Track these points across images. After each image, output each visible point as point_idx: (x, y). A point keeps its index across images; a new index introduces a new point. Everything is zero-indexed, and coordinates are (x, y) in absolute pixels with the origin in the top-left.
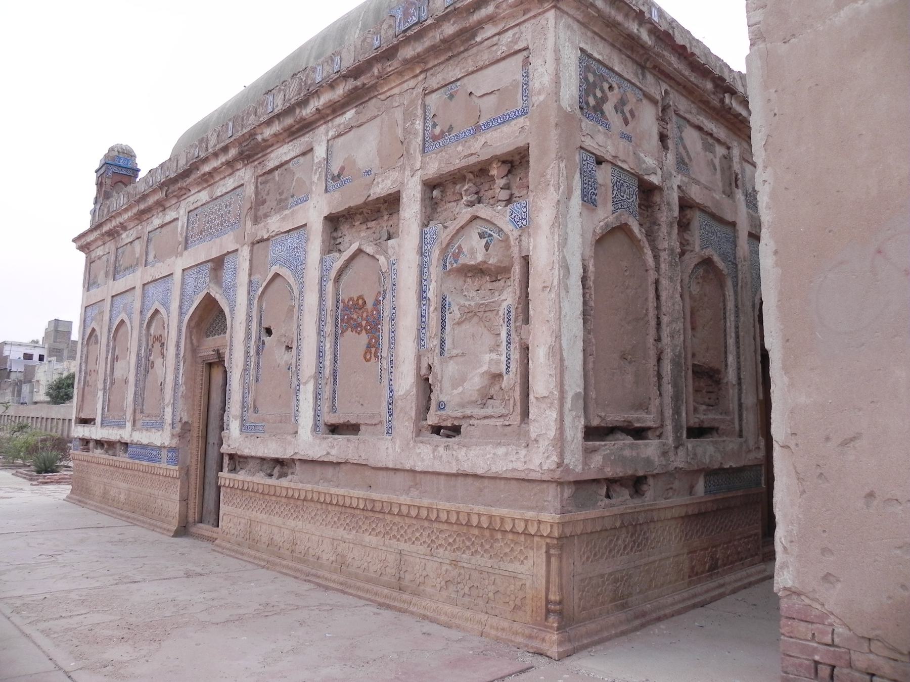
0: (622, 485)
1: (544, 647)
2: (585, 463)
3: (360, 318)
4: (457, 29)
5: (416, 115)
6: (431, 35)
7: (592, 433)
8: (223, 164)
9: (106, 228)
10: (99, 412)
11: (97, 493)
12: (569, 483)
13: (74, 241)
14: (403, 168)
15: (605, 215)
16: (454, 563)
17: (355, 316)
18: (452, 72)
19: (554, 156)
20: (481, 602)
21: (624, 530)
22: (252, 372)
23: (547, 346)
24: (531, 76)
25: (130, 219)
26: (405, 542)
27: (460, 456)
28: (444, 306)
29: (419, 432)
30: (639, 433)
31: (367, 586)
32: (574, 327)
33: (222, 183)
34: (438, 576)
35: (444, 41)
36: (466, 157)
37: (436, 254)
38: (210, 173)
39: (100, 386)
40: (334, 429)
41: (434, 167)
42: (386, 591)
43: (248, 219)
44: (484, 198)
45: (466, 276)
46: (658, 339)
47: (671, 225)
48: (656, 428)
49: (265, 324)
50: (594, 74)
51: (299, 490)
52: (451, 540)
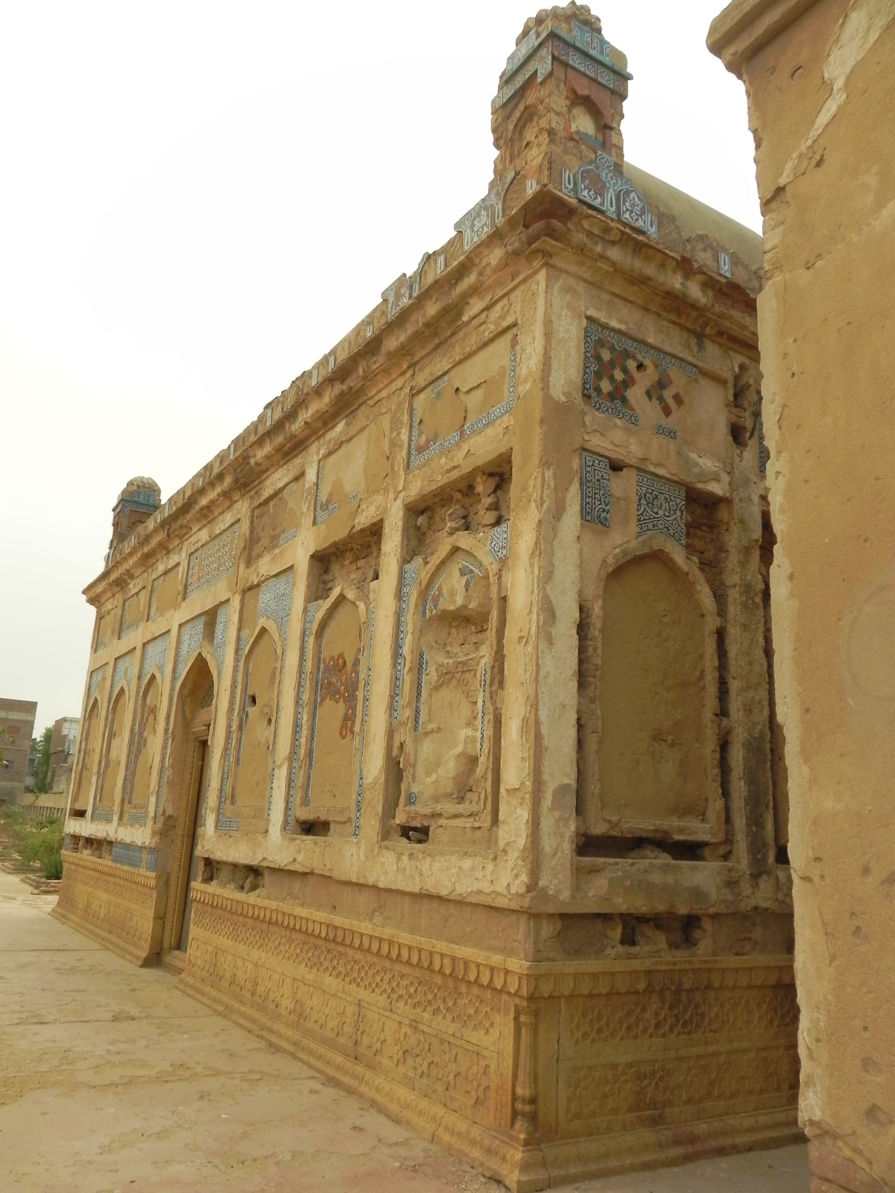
0: (658, 927)
2: (577, 887)
3: (335, 681)
4: (440, 307)
5: (402, 423)
6: (414, 318)
7: (588, 845)
8: (219, 495)
9: (113, 577)
10: (91, 802)
11: (80, 906)
12: (551, 916)
13: (84, 592)
14: (386, 491)
15: (623, 538)
16: (414, 1024)
17: (334, 680)
19: (536, 462)
20: (440, 1088)
21: (655, 997)
22: (233, 752)
23: (521, 718)
24: (518, 360)
25: (137, 565)
26: (365, 989)
27: (424, 869)
28: (420, 667)
29: (385, 835)
30: (690, 850)
31: (322, 1050)
32: (563, 690)
33: (221, 518)
34: (397, 1041)
35: (427, 325)
36: (448, 471)
39: (95, 770)
41: (416, 487)
42: (339, 1059)
43: (242, 560)
44: (473, 523)
45: (450, 626)
46: (723, 712)
47: (747, 551)
48: (717, 845)
49: (250, 692)
50: (612, 349)
51: (265, 909)
52: (412, 990)
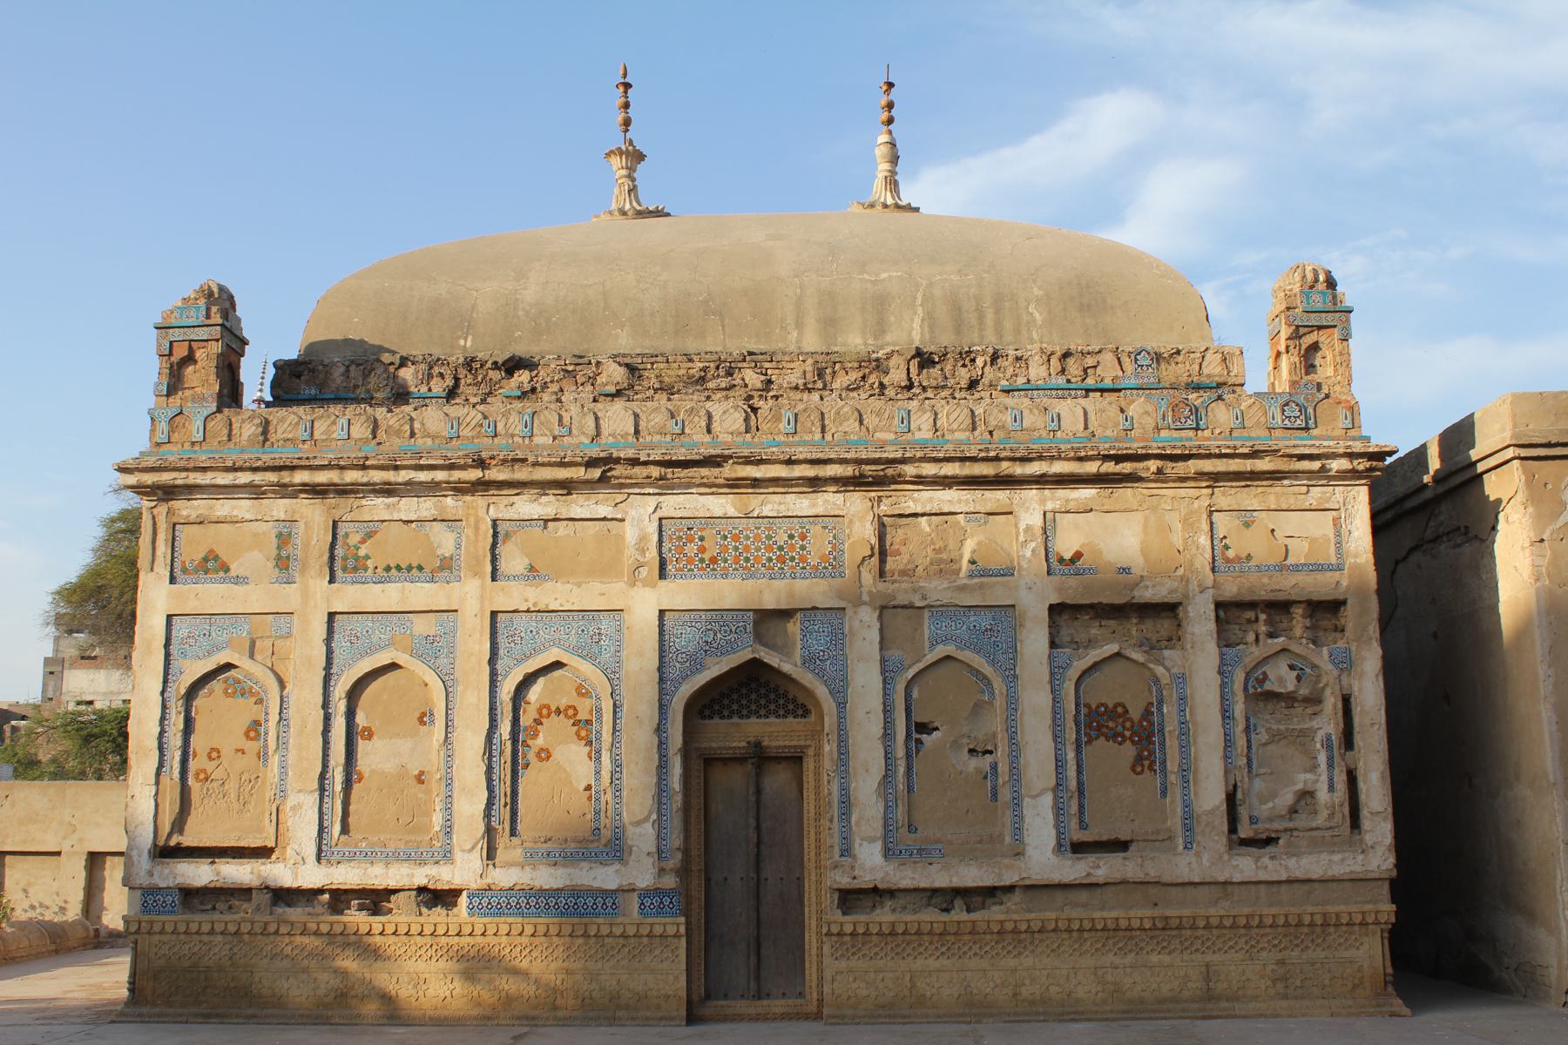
40: (1079, 848)
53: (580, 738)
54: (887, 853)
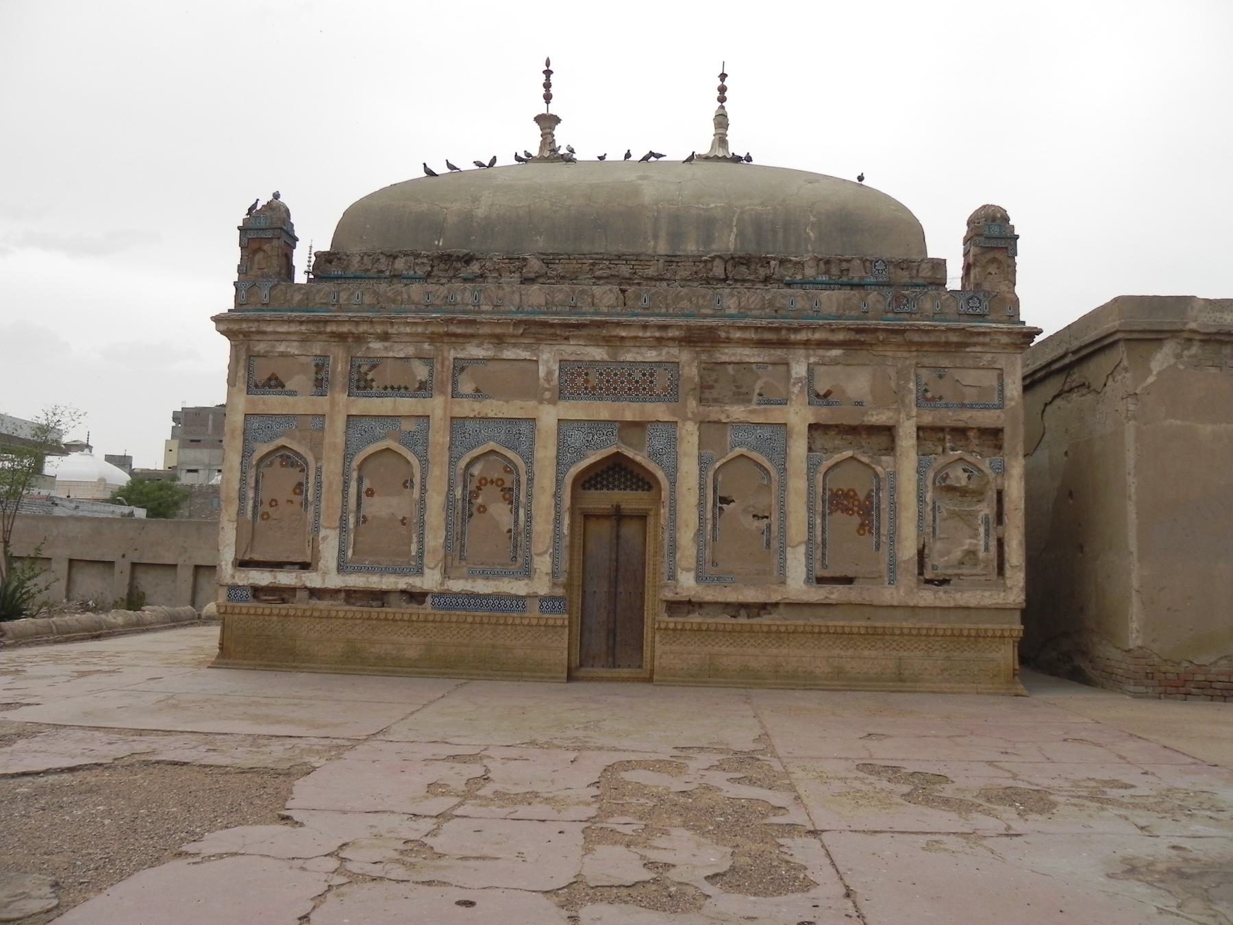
1: (1019, 692)
18: (944, 362)
37: (931, 475)
38: (623, 337)
40: (821, 581)
41: (928, 419)
53: (505, 499)
54: (698, 579)
